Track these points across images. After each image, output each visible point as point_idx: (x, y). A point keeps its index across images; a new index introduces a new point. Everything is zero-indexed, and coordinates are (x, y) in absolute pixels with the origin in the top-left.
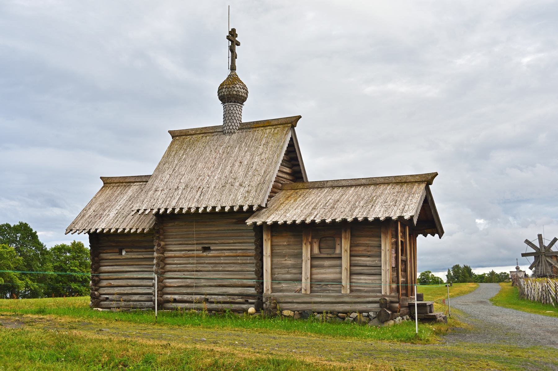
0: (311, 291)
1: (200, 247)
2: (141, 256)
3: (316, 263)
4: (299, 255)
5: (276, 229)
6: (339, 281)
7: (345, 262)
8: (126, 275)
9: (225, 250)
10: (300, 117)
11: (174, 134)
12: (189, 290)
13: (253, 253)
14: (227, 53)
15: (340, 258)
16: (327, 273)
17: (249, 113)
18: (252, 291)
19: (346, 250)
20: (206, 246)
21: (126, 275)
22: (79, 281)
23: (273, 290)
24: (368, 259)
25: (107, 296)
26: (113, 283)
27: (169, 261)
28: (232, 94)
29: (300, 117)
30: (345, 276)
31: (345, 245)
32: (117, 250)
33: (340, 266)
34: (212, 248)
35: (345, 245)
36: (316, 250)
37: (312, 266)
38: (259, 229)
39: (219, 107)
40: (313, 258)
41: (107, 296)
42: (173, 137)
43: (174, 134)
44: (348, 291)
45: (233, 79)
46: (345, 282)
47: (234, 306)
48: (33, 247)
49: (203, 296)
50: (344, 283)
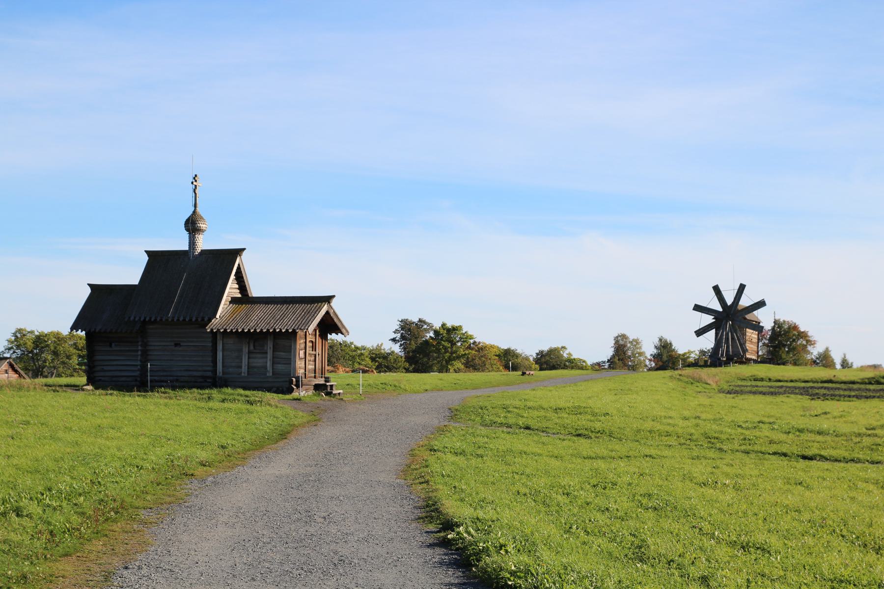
0: (248, 374)
3: (251, 355)
4: (241, 351)
6: (266, 368)
7: (270, 355)
10: (334, 296)
11: (91, 286)
12: (165, 374)
14: (192, 194)
15: (266, 353)
16: (258, 362)
17: (204, 243)
18: (209, 374)
26: (105, 368)
28: (192, 226)
29: (334, 296)
30: (269, 364)
31: (270, 345)
35: (270, 345)
36: (252, 348)
37: (249, 358)
38: (214, 334)
39: (186, 235)
40: (249, 352)
43: (91, 286)
45: (194, 212)
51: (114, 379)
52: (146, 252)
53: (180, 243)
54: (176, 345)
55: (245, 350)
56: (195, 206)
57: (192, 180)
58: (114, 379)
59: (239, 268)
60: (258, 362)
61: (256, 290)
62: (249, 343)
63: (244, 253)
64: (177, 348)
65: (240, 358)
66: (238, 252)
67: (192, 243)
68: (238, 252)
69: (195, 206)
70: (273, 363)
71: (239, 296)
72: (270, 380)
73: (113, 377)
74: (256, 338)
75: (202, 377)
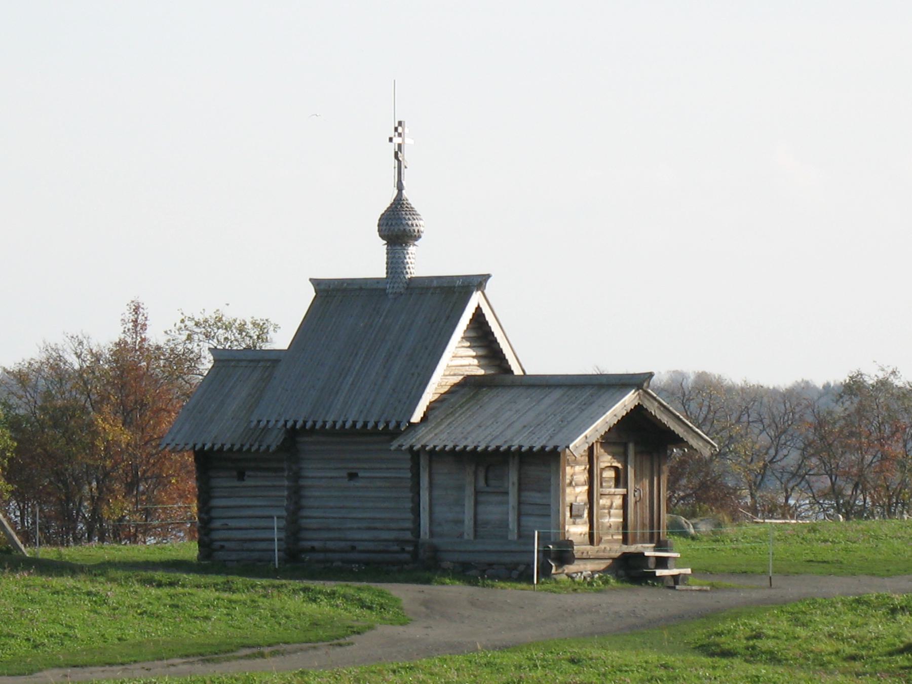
0: (476, 536)
1: (344, 473)
2: (269, 484)
3: (482, 498)
4: (461, 488)
5: (435, 455)
6: (504, 524)
7: (512, 498)
8: (249, 512)
9: (376, 478)
11: (316, 283)
13: (409, 484)
15: (507, 493)
16: (492, 512)
17: (422, 262)
18: (408, 536)
19: (513, 484)
20: (354, 471)
21: (249, 512)
22: (850, 673)
23: (432, 534)
24: (539, 495)
25: (222, 543)
26: (232, 523)
27: (305, 513)
28: (397, 229)
31: (513, 477)
32: (235, 473)
33: (507, 503)
34: (360, 475)
35: (513, 477)
36: (482, 483)
37: (476, 503)
38: (415, 455)
39: (381, 247)
40: (477, 493)
41: (222, 543)
42: (316, 291)
43: (316, 283)
44: (516, 537)
46: (513, 525)
47: (387, 557)
48: (180, 531)
49: (349, 543)
50: (511, 527)
51: (247, 545)
52: (311, 280)
53: (368, 261)
54: (353, 476)
55: (469, 491)
56: (400, 187)
57: (392, 133)
58: (247, 545)
59: (479, 315)
60: (492, 512)
61: (529, 356)
62: (476, 474)
63: (490, 283)
64: (352, 483)
65: (459, 503)
66: (478, 282)
67: (395, 263)
68: (478, 282)
69: (400, 187)
70: (519, 515)
71: (481, 372)
72: (513, 547)
73: (245, 541)
74: (489, 462)
75: (396, 541)
